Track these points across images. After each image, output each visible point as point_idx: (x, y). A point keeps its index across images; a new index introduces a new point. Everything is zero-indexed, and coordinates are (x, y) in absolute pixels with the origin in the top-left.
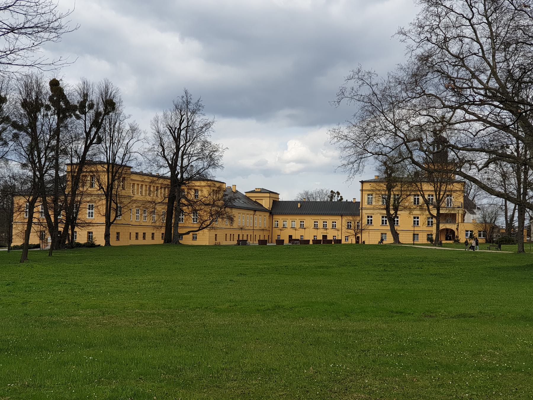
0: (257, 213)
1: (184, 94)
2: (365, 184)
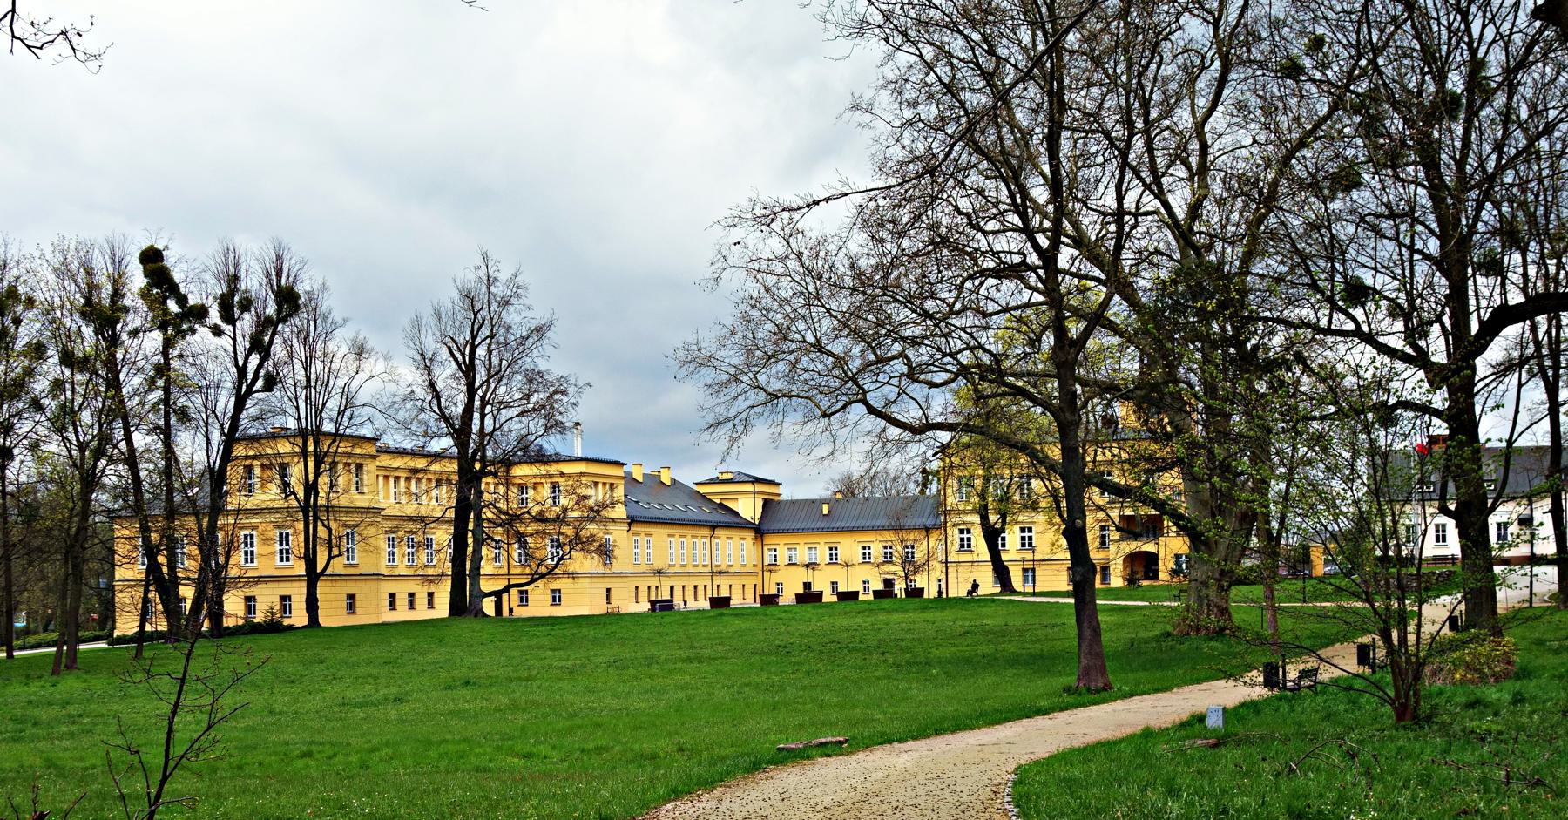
0: (718, 532)
1: (480, 262)
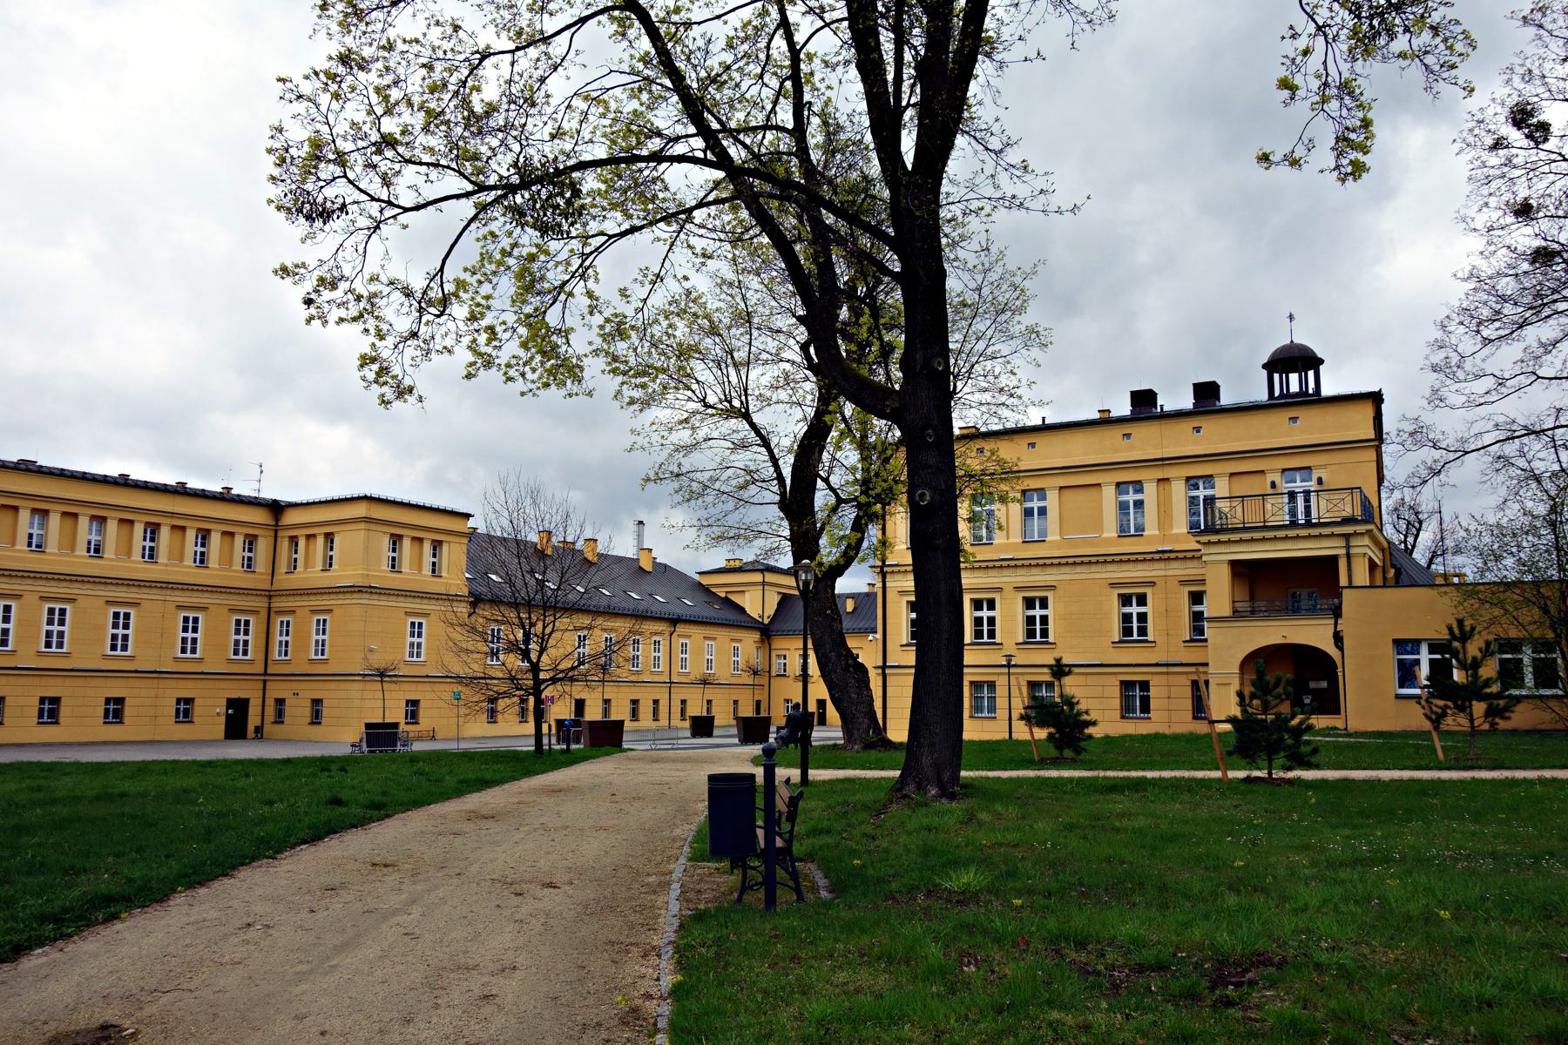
0: (680, 629)
2: (1368, 410)
